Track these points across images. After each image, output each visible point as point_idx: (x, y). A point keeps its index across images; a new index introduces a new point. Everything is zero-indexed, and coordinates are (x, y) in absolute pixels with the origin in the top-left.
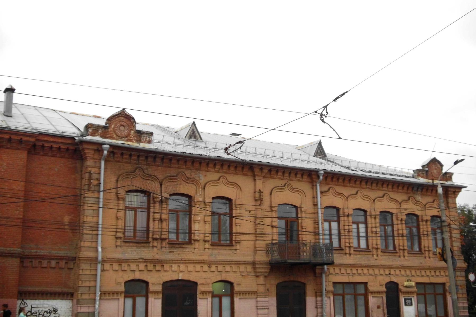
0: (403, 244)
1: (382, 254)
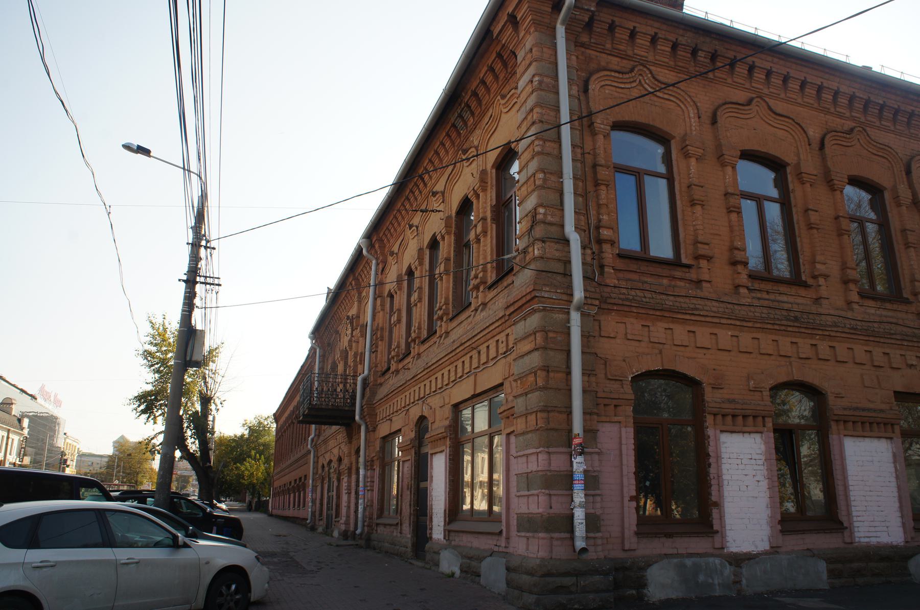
1: (620, 264)
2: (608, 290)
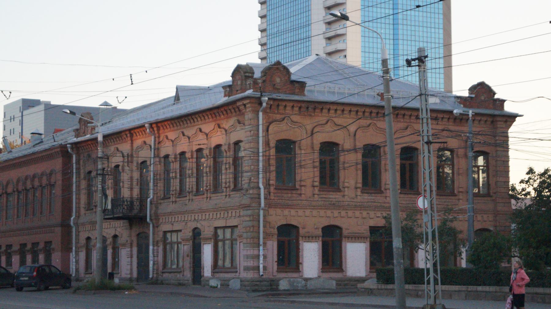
1: (276, 191)
2: (271, 201)
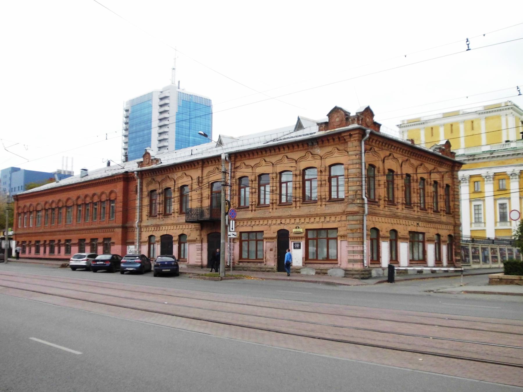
0: (276, 198)
